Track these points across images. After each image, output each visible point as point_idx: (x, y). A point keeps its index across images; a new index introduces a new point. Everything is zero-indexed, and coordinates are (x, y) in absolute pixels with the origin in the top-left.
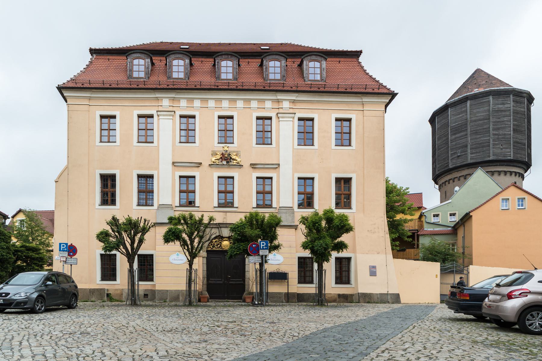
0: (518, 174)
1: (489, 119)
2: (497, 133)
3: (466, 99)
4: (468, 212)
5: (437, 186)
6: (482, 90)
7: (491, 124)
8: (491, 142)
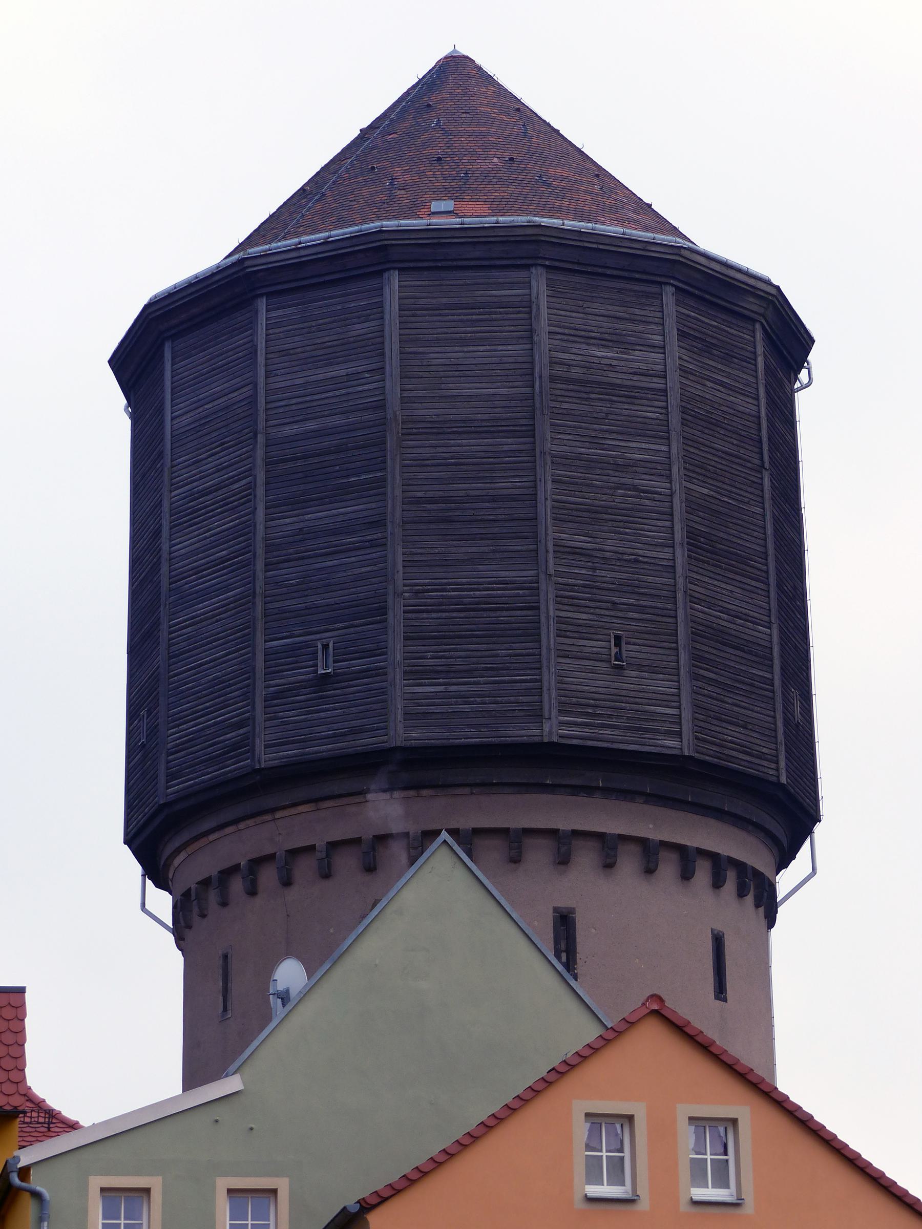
0: (731, 878)
1: (531, 432)
2: (582, 542)
3: (373, 257)
4: (350, 1201)
5: (162, 902)
6: (478, 217)
7: (547, 474)
8: (550, 609)
